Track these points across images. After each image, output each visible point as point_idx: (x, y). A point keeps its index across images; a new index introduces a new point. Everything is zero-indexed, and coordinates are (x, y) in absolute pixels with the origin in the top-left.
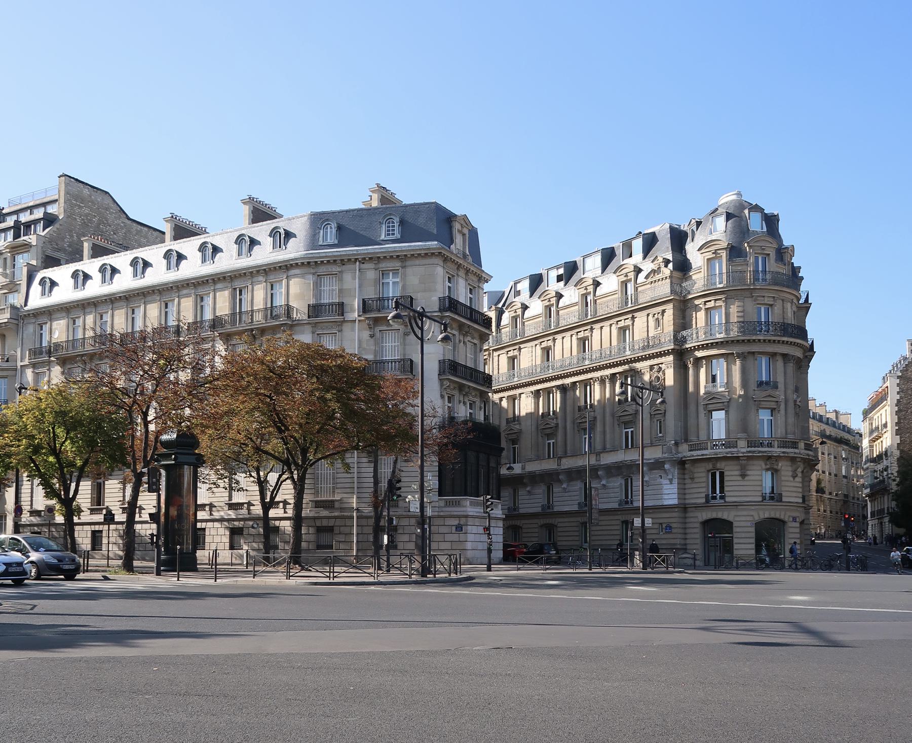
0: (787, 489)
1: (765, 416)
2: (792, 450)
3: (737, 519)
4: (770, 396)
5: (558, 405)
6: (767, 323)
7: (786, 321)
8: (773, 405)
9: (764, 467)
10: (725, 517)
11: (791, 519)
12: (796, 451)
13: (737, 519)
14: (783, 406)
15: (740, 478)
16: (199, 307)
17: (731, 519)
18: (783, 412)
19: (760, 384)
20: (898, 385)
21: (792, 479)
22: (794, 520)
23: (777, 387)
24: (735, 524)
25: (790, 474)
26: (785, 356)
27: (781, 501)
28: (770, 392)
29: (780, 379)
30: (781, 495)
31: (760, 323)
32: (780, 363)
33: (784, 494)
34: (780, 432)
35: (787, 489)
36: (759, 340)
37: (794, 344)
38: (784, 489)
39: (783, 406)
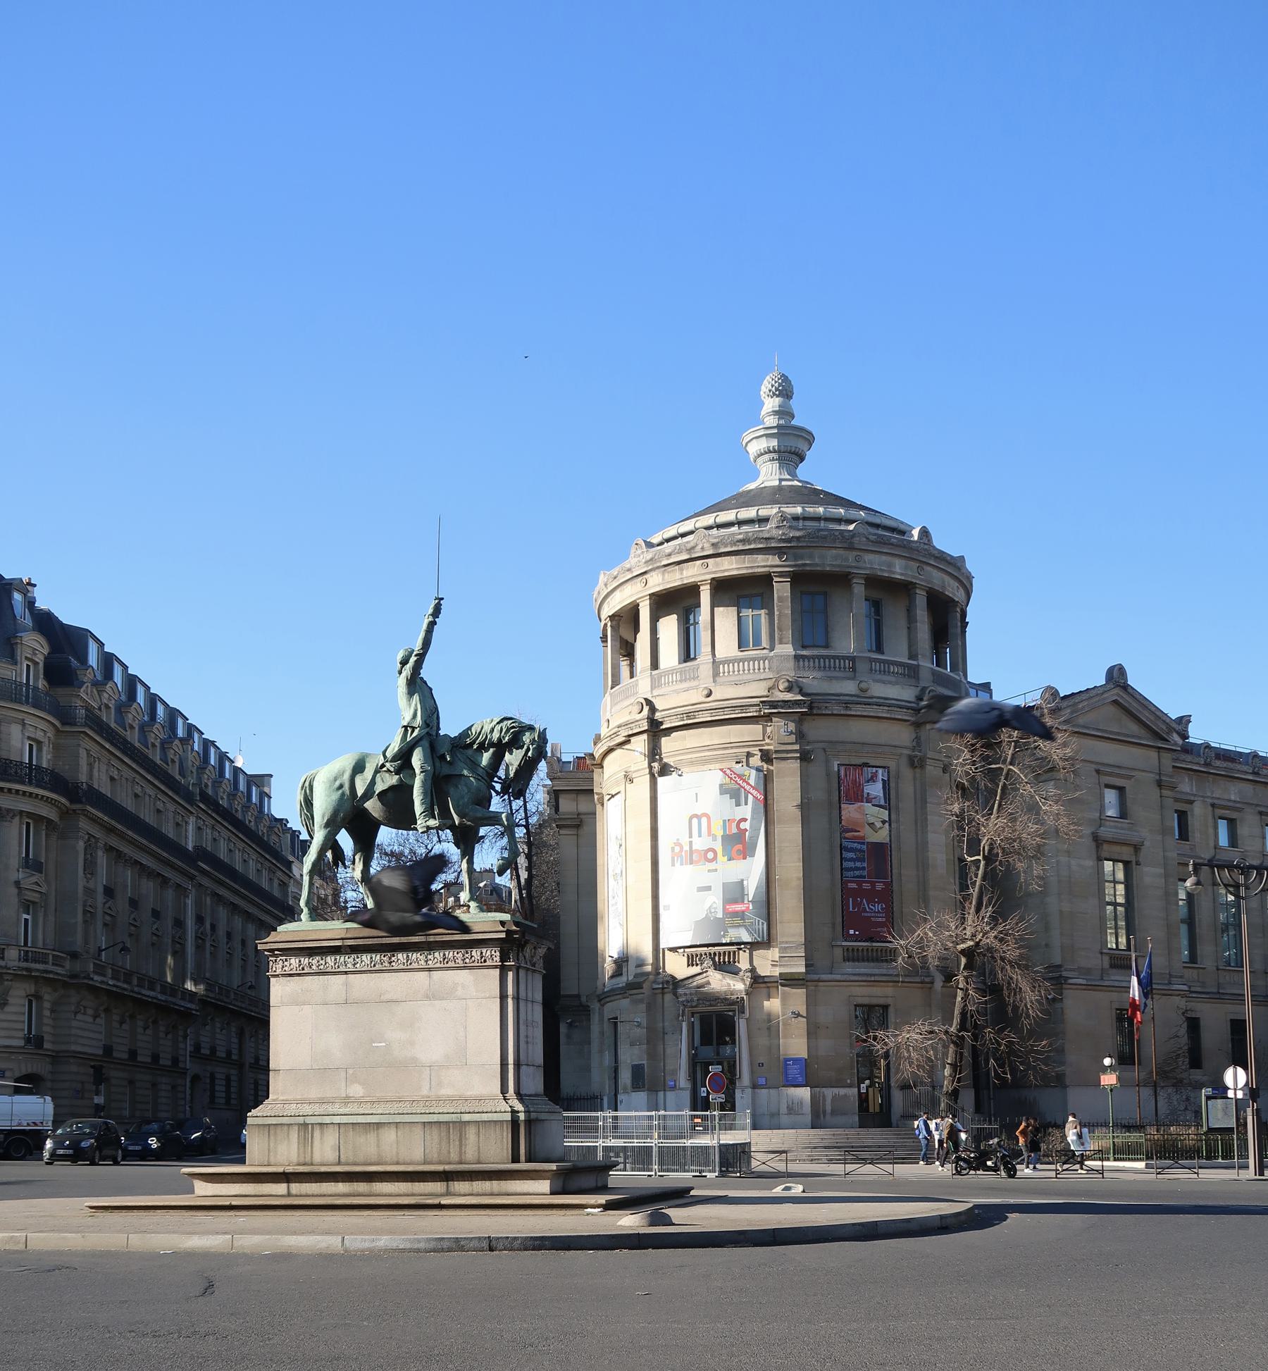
21: (91, 1020)
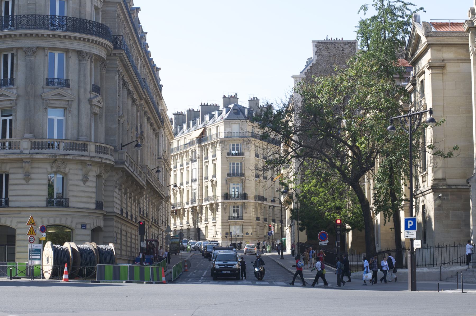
0: (75, 194)
1: (55, 115)
2: (81, 153)
3: (20, 225)
4: (59, 94)
5: (77, 158)
6: (61, 17)
7: (83, 17)
8: (64, 104)
9: (49, 170)
10: (8, 224)
11: (80, 226)
12: (86, 153)
13: (20, 225)
14: (74, 106)
15: (23, 182)
16: (124, 240)
17: (13, 226)
18: (75, 112)
19: (50, 82)
20: (270, 107)
21: (82, 183)
22: (84, 226)
23: (68, 86)
24: (18, 232)
25: (81, 177)
26: (79, 53)
27: (68, 206)
28: (60, 90)
29: (73, 78)
30: (67, 200)
31: (53, 17)
32: (74, 60)
33: (71, 199)
34: (71, 133)
35: (75, 194)
36: (48, 35)
37: (99, 43)
38: (71, 194)
39: (74, 106)
